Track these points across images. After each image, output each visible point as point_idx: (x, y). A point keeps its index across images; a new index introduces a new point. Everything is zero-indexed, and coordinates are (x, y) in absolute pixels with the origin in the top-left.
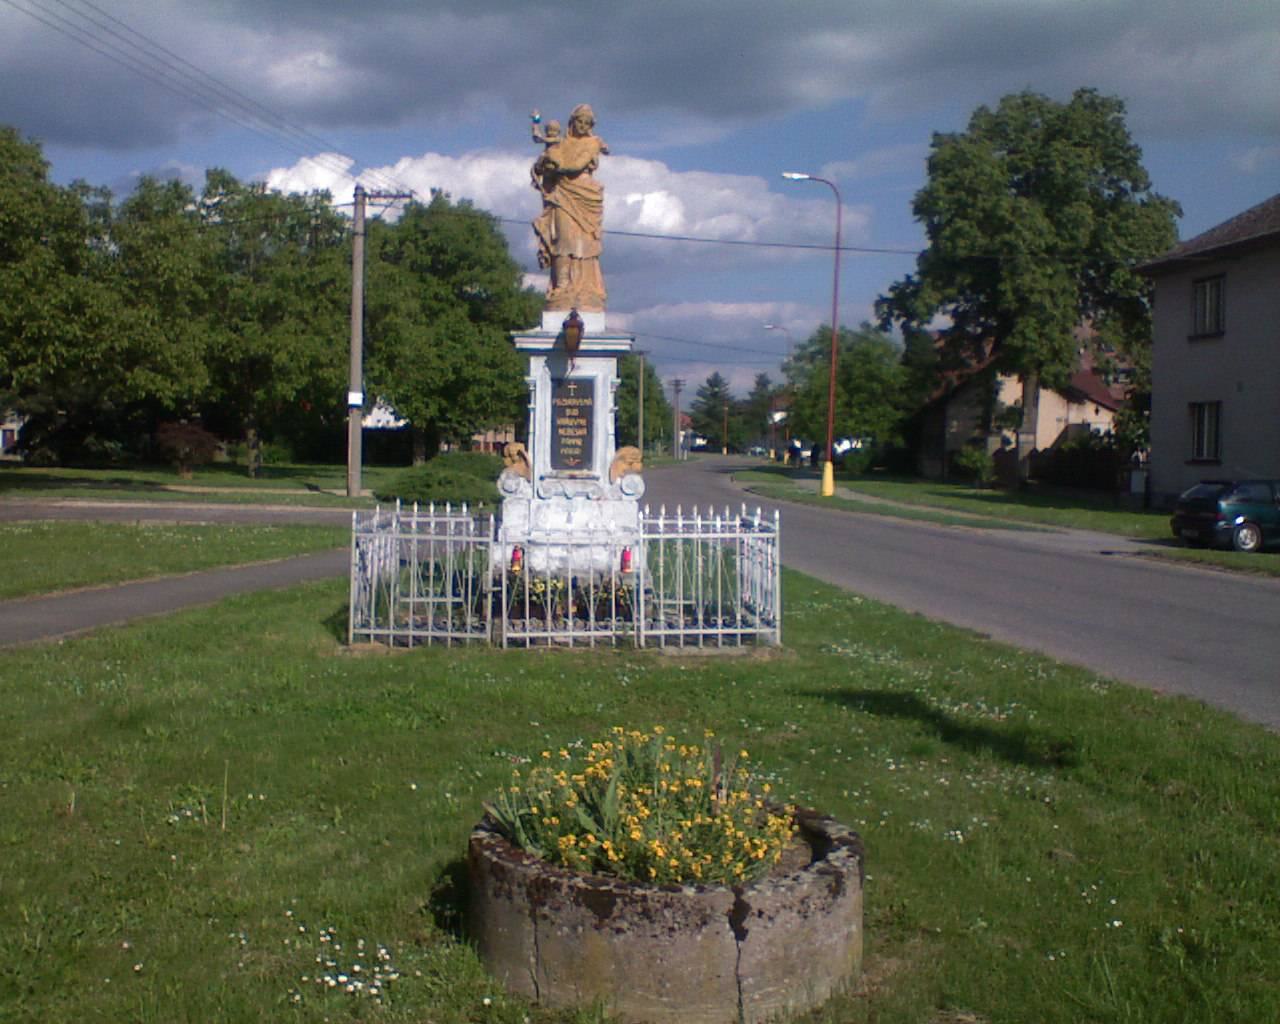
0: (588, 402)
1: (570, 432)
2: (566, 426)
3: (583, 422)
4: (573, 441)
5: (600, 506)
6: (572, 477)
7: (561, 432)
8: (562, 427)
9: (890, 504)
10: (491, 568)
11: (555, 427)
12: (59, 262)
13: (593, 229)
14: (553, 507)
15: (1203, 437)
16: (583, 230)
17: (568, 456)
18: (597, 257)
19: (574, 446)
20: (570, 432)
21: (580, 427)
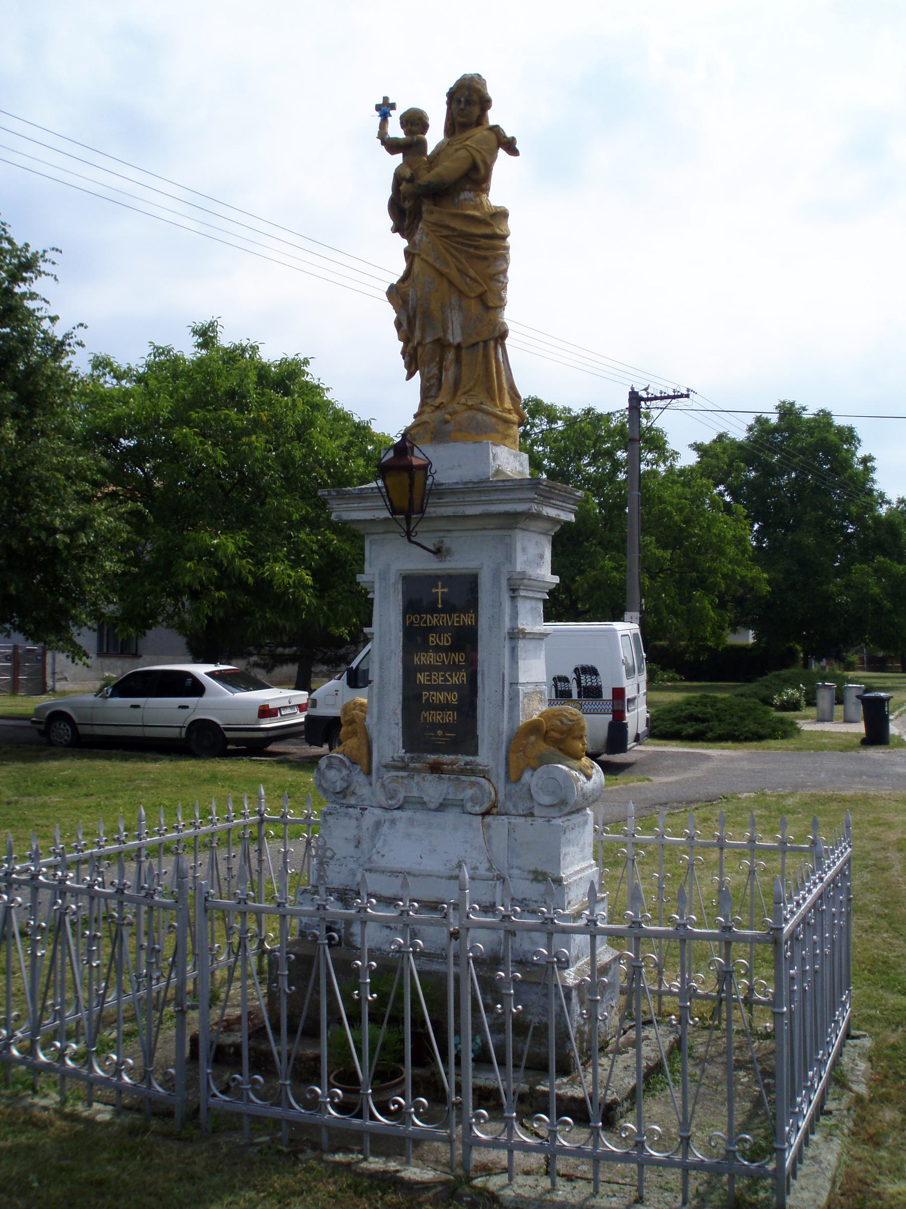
0: (467, 620)
1: (438, 678)
2: (430, 668)
3: (459, 658)
4: (441, 697)
5: (487, 827)
6: (436, 768)
7: (421, 678)
8: (422, 668)
9: (209, 929)
10: (573, 1034)
11: (409, 672)
12: (711, 1176)
13: (479, 291)
14: (400, 826)
15: (455, 996)
16: (461, 293)
17: (434, 726)
18: (514, 590)
19: (443, 707)
20: (438, 678)
21: (454, 667)
